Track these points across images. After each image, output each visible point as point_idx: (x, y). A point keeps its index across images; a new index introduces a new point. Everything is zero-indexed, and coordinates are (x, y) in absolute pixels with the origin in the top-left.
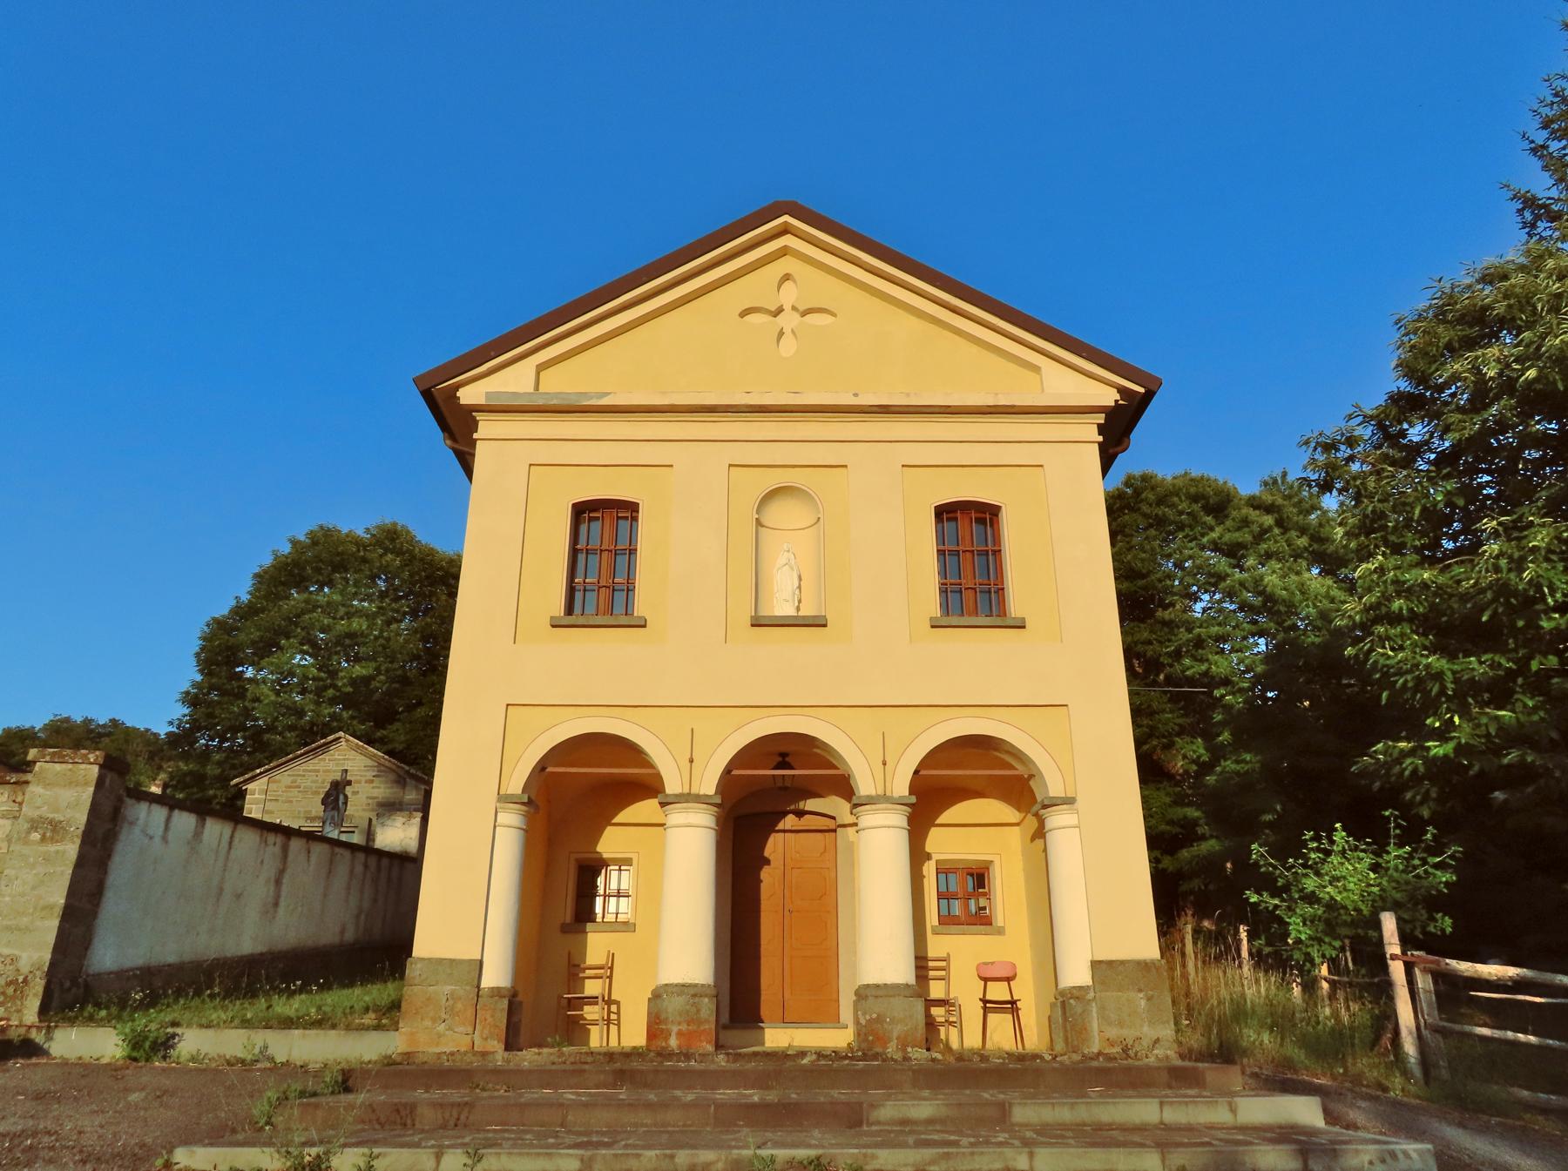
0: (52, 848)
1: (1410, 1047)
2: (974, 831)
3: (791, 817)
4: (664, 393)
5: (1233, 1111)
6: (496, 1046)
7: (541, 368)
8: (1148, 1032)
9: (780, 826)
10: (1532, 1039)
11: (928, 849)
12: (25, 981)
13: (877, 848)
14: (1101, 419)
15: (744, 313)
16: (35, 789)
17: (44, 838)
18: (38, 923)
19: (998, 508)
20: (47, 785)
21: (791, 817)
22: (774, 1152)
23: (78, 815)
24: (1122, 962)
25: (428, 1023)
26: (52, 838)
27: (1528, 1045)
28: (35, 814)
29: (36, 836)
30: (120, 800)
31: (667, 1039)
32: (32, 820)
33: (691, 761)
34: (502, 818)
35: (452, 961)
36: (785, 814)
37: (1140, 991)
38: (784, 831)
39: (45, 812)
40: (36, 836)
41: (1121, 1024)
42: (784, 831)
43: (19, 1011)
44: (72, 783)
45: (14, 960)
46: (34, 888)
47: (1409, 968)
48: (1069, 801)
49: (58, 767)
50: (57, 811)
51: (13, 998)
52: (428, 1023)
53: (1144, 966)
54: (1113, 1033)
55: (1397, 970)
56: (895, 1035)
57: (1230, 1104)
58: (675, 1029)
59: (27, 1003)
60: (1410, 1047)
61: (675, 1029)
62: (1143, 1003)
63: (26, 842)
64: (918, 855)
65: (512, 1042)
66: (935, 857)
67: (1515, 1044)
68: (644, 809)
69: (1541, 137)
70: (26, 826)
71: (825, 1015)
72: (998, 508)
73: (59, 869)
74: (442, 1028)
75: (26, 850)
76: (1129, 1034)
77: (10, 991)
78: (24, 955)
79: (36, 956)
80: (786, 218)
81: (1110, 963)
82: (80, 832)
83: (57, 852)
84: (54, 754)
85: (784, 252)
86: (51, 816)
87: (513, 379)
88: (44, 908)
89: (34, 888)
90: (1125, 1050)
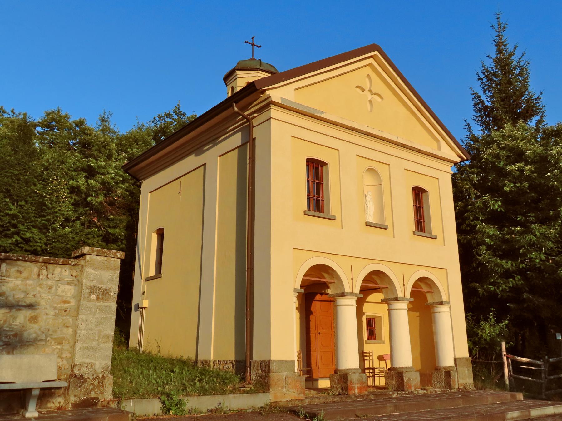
0: (103, 304)
1: (507, 382)
2: (374, 307)
4: (342, 118)
11: (364, 311)
12: (103, 377)
13: (347, 310)
15: (358, 87)
16: (89, 270)
17: (98, 298)
18: (102, 345)
19: (307, 159)
20: (96, 268)
23: (114, 286)
25: (280, 389)
26: (103, 299)
27: (530, 381)
28: (92, 284)
29: (94, 297)
31: (354, 390)
32: (90, 288)
33: (352, 279)
35: (286, 361)
36: (316, 294)
39: (95, 283)
40: (94, 297)
43: (102, 393)
44: (108, 268)
45: (92, 366)
46: (96, 326)
47: (508, 358)
48: (448, 303)
49: (98, 258)
50: (102, 283)
51: (98, 386)
52: (280, 389)
53: (466, 359)
55: (505, 359)
56: (413, 385)
58: (356, 386)
59: (106, 389)
60: (507, 382)
61: (356, 386)
63: (89, 300)
64: (360, 313)
66: (366, 314)
67: (528, 380)
69: (482, 76)
70: (88, 291)
72: (307, 159)
73: (109, 316)
74: (284, 390)
75: (89, 304)
77: (96, 382)
78: (97, 363)
79: (104, 363)
82: (116, 295)
83: (106, 306)
84: (98, 251)
86: (100, 286)
88: (104, 337)
89: (96, 326)
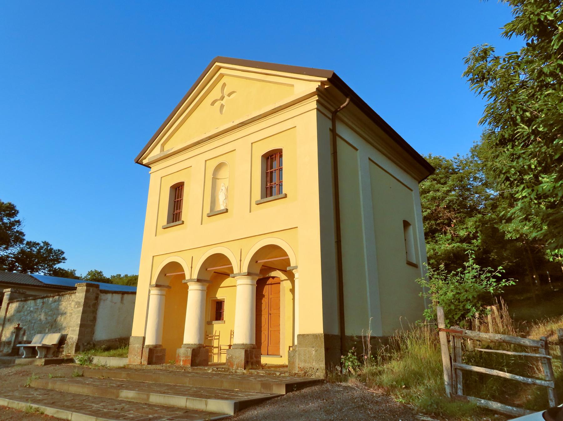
3: (271, 279)
5: (206, 405)
6: (145, 362)
7: (163, 146)
8: (315, 365)
9: (268, 283)
10: (508, 375)
14: (316, 98)
21: (271, 279)
22: (32, 405)
24: (308, 335)
30: (98, 294)
34: (152, 292)
37: (313, 347)
38: (269, 284)
41: (305, 361)
42: (269, 284)
54: (302, 365)
57: (206, 401)
62: (314, 352)
65: (150, 362)
68: (227, 282)
71: (277, 354)
76: (307, 365)
80: (217, 64)
81: (303, 335)
85: (222, 76)
87: (156, 152)
90: (305, 373)
